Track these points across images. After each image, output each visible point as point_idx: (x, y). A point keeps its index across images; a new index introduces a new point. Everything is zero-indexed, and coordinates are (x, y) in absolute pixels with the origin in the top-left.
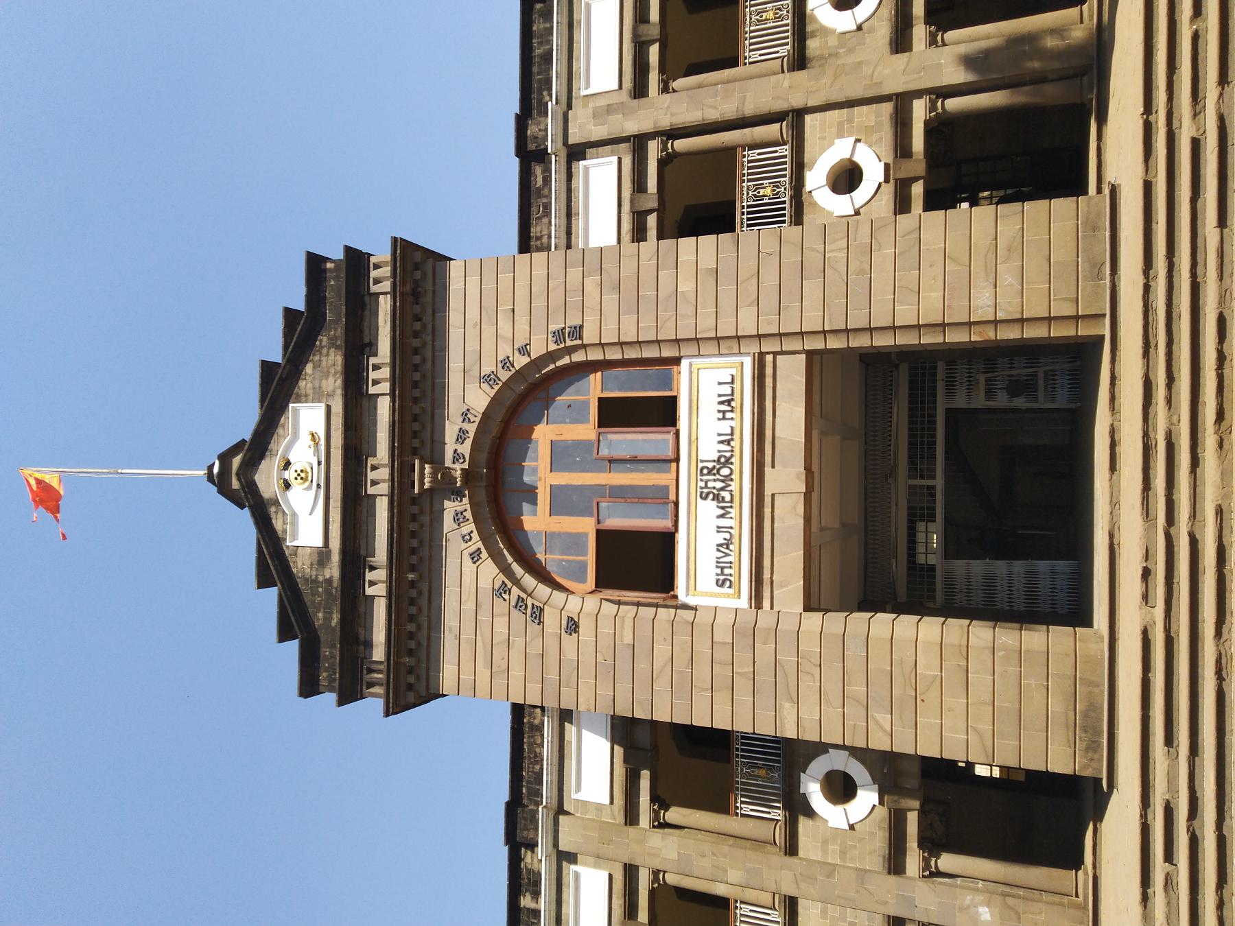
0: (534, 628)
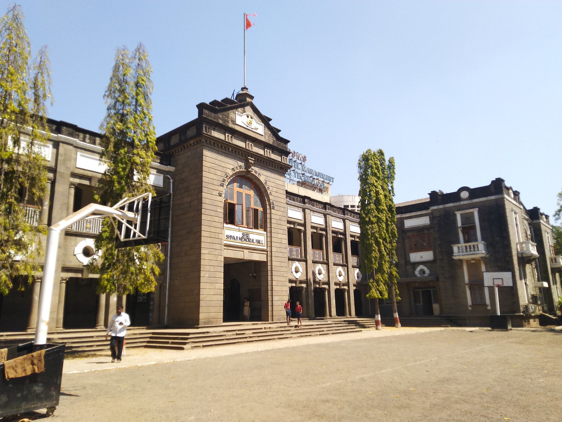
0: (219, 183)
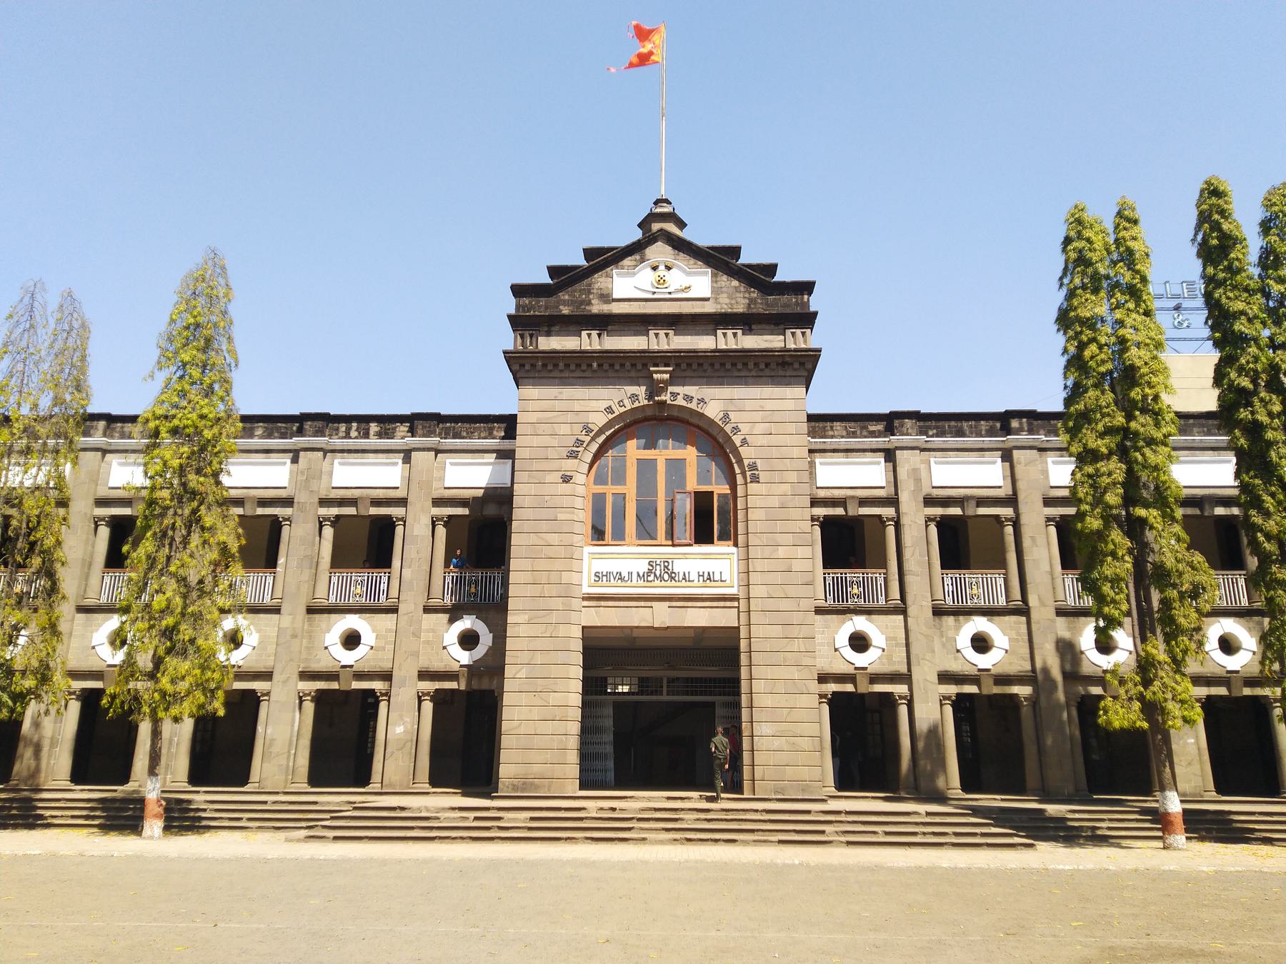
0: (564, 452)
